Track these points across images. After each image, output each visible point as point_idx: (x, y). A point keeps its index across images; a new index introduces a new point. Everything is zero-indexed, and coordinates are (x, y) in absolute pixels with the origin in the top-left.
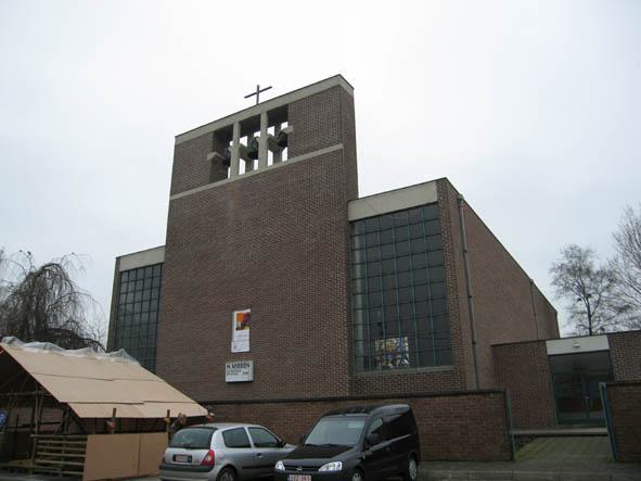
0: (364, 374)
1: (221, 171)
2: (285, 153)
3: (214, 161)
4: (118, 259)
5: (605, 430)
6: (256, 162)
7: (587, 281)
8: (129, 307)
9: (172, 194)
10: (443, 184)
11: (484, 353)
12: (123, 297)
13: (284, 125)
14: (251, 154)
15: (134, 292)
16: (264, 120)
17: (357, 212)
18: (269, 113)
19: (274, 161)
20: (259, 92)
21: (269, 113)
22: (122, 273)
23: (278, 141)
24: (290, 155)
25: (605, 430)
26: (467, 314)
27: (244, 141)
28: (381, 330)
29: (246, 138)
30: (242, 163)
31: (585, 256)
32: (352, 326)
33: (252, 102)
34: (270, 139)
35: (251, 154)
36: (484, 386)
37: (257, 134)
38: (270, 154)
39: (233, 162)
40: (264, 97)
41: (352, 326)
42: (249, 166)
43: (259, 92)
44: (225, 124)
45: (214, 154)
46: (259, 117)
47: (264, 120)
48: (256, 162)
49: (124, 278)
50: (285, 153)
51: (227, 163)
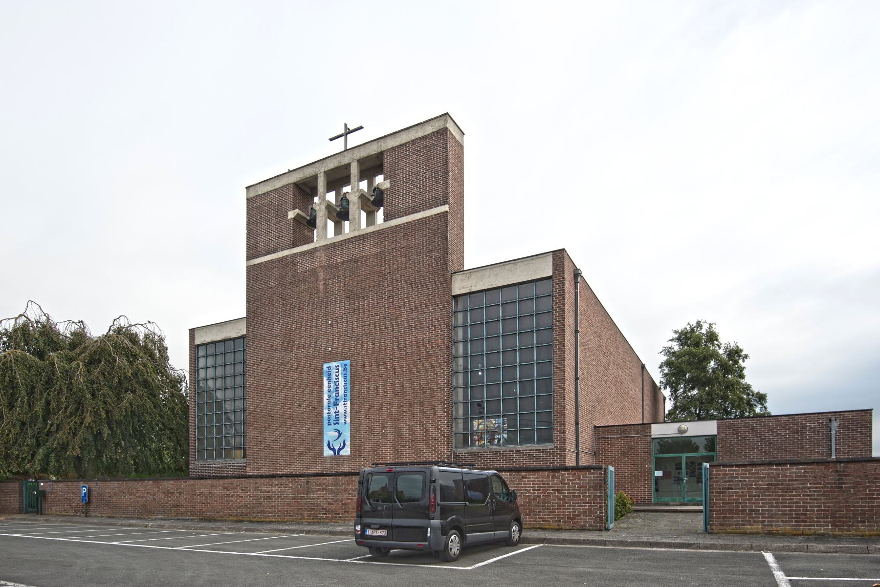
0: (463, 450)
1: (306, 233)
2: (380, 215)
3: (297, 219)
4: (192, 332)
5: (701, 508)
6: (346, 224)
7: (127, 474)
8: (211, 383)
9: (249, 258)
10: (559, 257)
11: (586, 436)
12: (202, 374)
13: (379, 179)
14: (341, 215)
15: (206, 368)
16: (354, 170)
17: (459, 286)
18: (361, 162)
19: (336, 234)
20: (348, 132)
21: (361, 162)
22: (198, 346)
23: (372, 199)
24: (387, 218)
25: (701, 508)
26: (573, 396)
27: (331, 197)
28: (478, 410)
29: (333, 193)
30: (331, 225)
31: (674, 353)
32: (451, 404)
33: (338, 146)
34: (362, 197)
35: (341, 215)
36: (584, 461)
37: (347, 189)
38: (363, 215)
39: (319, 222)
40: (354, 140)
41: (451, 404)
42: (338, 229)
43: (348, 132)
44: (309, 172)
45: (297, 211)
46: (315, 178)
47: (354, 170)
48: (346, 224)
49: (201, 353)
50: (380, 215)
51: (312, 223)
